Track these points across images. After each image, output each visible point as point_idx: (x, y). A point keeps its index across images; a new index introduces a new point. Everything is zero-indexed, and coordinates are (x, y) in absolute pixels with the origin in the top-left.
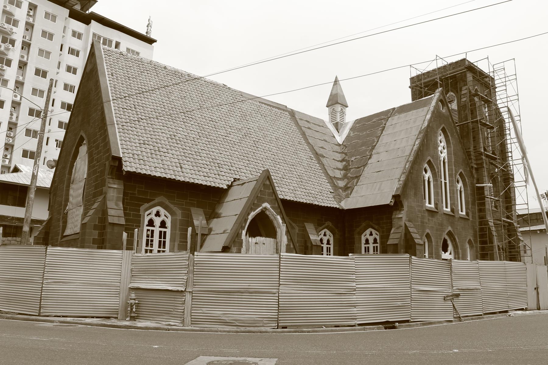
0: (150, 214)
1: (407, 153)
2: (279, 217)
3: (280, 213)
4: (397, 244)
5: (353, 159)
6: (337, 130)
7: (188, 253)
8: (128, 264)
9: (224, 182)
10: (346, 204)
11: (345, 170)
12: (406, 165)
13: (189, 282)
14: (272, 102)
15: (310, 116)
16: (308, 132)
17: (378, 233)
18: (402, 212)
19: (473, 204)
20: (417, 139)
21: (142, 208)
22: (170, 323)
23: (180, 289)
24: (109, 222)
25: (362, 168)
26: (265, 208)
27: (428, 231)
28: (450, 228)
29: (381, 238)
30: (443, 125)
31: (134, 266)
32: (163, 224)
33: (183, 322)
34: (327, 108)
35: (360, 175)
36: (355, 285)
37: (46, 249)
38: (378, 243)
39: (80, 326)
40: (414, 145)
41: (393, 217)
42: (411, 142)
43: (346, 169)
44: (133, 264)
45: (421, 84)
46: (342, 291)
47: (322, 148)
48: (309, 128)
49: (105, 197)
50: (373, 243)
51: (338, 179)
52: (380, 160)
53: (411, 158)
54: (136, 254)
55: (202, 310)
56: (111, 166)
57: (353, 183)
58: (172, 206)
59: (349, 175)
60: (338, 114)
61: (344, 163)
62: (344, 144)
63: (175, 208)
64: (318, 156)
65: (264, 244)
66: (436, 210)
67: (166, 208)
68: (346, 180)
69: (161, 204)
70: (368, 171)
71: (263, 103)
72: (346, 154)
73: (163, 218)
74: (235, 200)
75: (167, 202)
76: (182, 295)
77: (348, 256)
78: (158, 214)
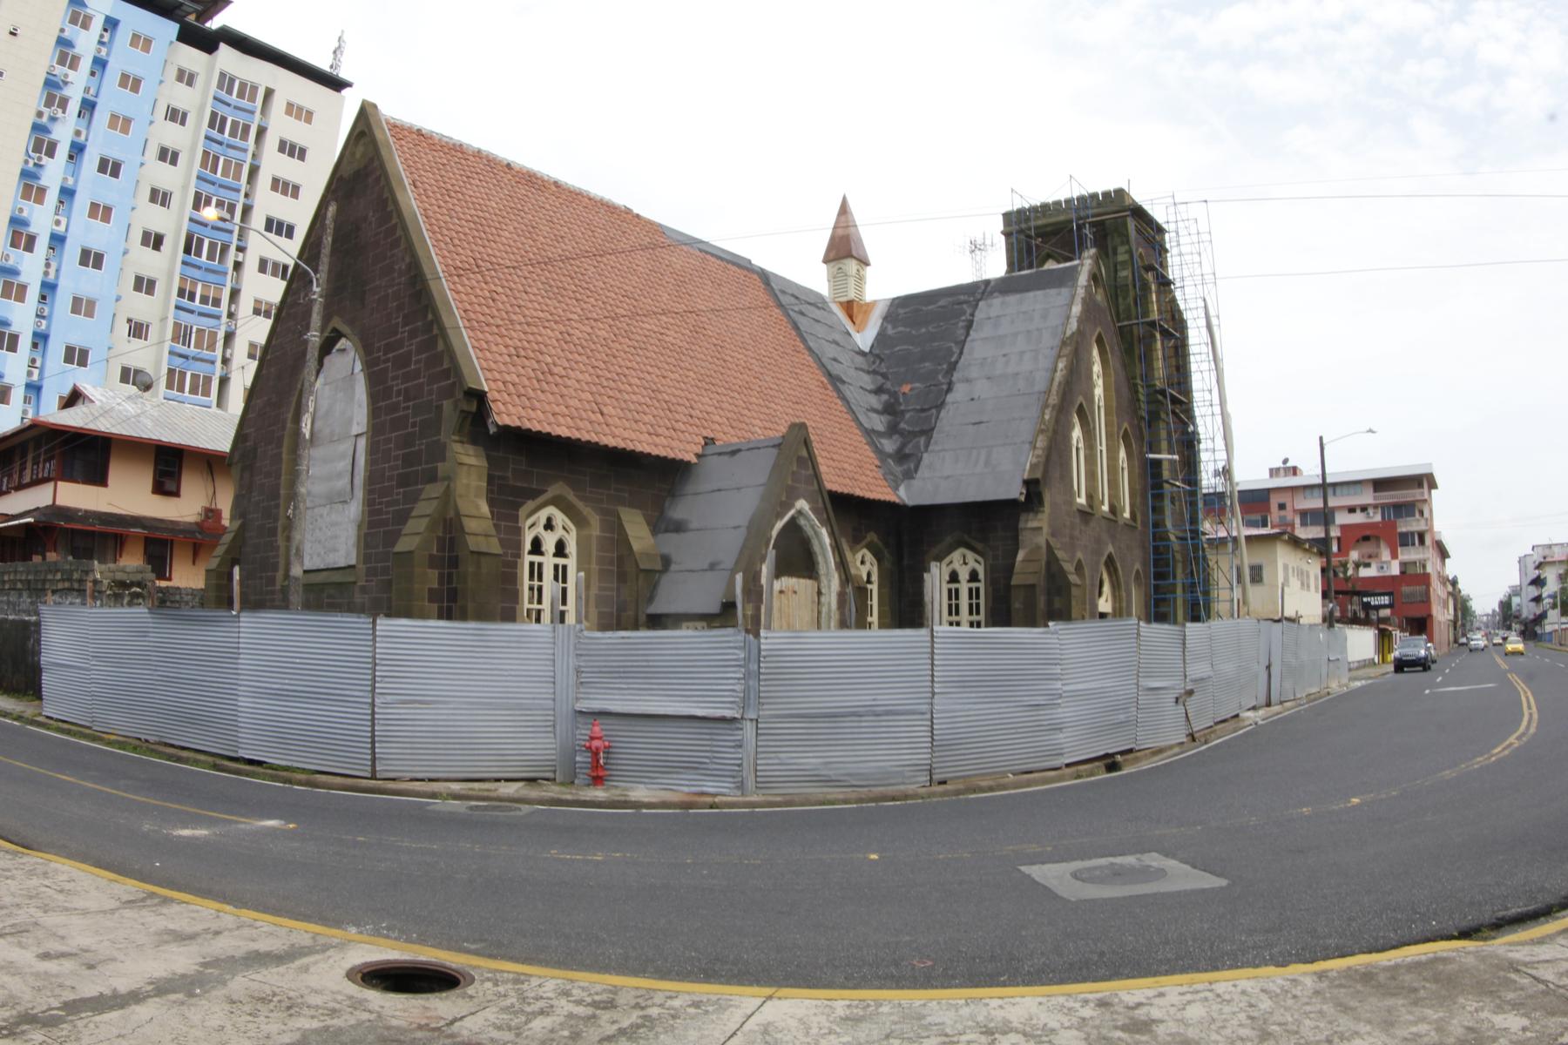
0: (533, 525)
1: (1040, 385)
2: (824, 532)
3: (827, 522)
4: (1033, 586)
5: (906, 388)
6: (851, 317)
7: (739, 631)
8: (568, 656)
9: (688, 447)
10: (906, 495)
11: (889, 414)
12: (1043, 414)
13: (749, 698)
14: (723, 251)
15: (796, 284)
16: (804, 323)
17: (980, 559)
18: (1040, 516)
19: (1144, 497)
20: (1059, 356)
21: (522, 512)
22: (705, 789)
23: (728, 713)
24: (472, 549)
25: (934, 411)
26: (800, 512)
27: (1079, 555)
28: (1110, 549)
29: (990, 571)
30: (1099, 329)
31: (585, 661)
32: (560, 550)
33: (741, 786)
34: (825, 266)
35: (933, 429)
36: (1060, 686)
37: (374, 623)
38: (979, 581)
39: (526, 808)
40: (1055, 371)
41: (1021, 525)
42: (1045, 363)
43: (890, 409)
44: (581, 655)
45: (1030, 229)
46: (1041, 700)
47: (835, 360)
48: (802, 313)
49: (448, 486)
50: (969, 581)
51: (880, 434)
52: (976, 397)
53: (1054, 399)
54: (586, 633)
55: (779, 758)
56: (462, 411)
57: (917, 446)
58: (580, 505)
59: (902, 425)
60: (852, 282)
61: (885, 397)
62: (876, 351)
63: (587, 510)
64: (835, 380)
65: (795, 592)
66: (1090, 511)
67: (568, 510)
68: (896, 437)
69: (558, 502)
70: (949, 419)
71: (707, 253)
72: (884, 376)
73: (559, 533)
74: (719, 490)
75: (571, 496)
76: (733, 726)
77: (1048, 626)
78: (549, 526)
